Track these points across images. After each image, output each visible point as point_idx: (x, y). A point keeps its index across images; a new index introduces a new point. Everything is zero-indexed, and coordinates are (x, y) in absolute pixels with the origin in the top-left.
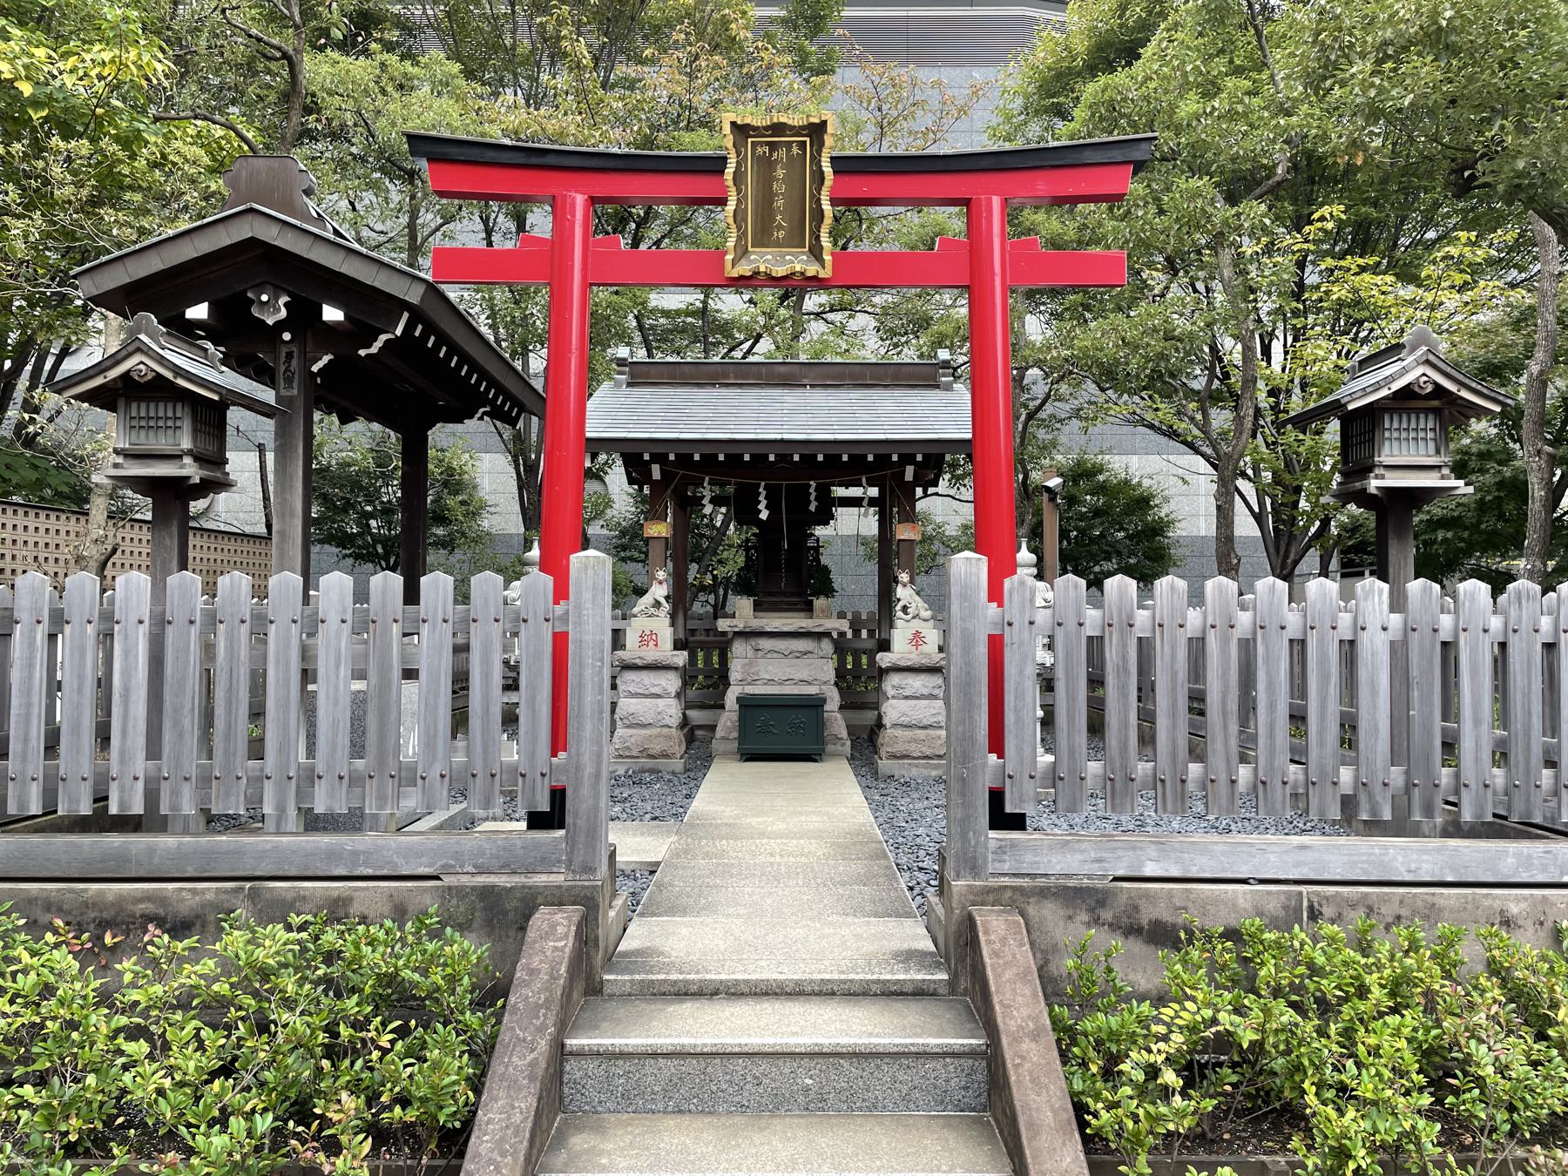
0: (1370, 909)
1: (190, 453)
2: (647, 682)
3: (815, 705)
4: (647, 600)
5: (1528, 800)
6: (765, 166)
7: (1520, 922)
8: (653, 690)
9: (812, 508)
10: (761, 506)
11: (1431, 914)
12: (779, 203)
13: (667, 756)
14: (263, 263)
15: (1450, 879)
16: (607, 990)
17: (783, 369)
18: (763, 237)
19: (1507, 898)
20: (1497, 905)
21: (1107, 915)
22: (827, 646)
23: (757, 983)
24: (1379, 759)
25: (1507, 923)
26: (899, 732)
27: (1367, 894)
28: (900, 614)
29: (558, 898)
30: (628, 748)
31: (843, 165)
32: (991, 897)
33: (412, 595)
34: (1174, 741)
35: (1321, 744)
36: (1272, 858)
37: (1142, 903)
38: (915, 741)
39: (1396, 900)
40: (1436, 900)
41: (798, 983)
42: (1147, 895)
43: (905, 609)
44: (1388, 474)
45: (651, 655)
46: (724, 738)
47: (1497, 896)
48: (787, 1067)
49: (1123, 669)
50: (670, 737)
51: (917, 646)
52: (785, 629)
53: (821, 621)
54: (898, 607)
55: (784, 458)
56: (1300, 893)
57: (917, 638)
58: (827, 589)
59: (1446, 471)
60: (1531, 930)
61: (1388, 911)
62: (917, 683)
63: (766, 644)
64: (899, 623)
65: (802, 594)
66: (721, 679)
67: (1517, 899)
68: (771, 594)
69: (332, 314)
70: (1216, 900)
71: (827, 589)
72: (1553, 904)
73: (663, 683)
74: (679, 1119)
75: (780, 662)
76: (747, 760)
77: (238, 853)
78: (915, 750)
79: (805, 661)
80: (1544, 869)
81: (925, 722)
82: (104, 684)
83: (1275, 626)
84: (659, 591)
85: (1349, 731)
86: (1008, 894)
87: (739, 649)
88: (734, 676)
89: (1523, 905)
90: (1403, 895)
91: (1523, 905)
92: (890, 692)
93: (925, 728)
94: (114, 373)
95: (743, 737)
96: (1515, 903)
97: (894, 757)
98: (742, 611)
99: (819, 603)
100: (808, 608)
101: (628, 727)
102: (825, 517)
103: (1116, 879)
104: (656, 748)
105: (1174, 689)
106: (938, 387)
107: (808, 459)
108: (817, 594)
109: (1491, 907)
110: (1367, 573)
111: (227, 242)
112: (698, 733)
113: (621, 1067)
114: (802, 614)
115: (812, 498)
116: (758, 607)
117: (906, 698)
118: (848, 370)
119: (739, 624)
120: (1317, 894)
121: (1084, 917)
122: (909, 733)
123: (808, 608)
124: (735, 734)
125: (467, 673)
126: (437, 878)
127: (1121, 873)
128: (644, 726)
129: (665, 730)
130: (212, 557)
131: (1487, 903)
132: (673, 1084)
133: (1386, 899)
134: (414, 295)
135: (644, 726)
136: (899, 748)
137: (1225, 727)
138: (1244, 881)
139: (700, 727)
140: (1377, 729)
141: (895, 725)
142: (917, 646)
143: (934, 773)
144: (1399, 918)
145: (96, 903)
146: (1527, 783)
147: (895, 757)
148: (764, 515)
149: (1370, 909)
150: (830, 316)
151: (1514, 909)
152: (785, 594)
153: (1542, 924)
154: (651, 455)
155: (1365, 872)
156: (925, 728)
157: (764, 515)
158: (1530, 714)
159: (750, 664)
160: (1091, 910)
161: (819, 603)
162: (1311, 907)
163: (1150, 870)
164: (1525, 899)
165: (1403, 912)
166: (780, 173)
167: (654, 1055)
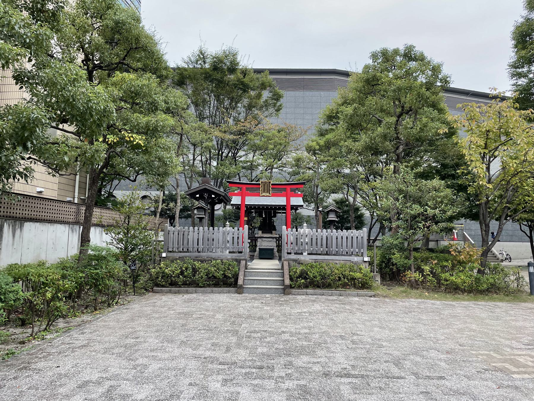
3: (273, 249)
6: (264, 185)
14: (206, 190)
22: (275, 240)
29: (243, 260)
31: (272, 184)
33: (213, 230)
55: (267, 208)
58: (275, 230)
63: (264, 239)
66: (256, 246)
69: (213, 196)
71: (275, 230)
75: (266, 242)
82: (198, 239)
85: (322, 245)
87: (259, 240)
88: (258, 245)
98: (259, 233)
99: (273, 232)
100: (271, 233)
102: (275, 216)
107: (271, 208)
119: (259, 236)
130: (49, 212)
134: (224, 195)
161: (273, 232)
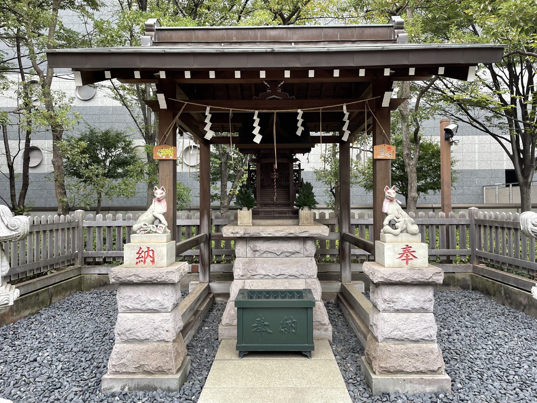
2: (143, 298)
4: (146, 217)
8: (151, 306)
9: (299, 133)
10: (256, 132)
13: (163, 372)
26: (392, 346)
28: (387, 228)
30: (124, 365)
38: (408, 355)
43: (392, 224)
45: (146, 272)
46: (228, 325)
50: (165, 353)
51: (407, 260)
52: (277, 235)
53: (307, 228)
54: (386, 222)
57: (407, 253)
62: (408, 297)
63: (262, 246)
64: (388, 237)
65: (289, 205)
68: (266, 205)
73: (159, 298)
75: (275, 262)
76: (245, 356)
78: (407, 364)
79: (294, 259)
81: (418, 336)
84: (159, 208)
92: (381, 305)
93: (417, 341)
95: (241, 337)
97: (388, 372)
99: (304, 212)
101: (127, 341)
104: (152, 364)
108: (301, 205)
110: (511, 185)
112: (218, 299)
114: (290, 222)
115: (299, 124)
116: (256, 215)
117: (397, 311)
119: (240, 231)
122: (400, 347)
123: (295, 215)
124: (235, 322)
125: (261, 188)
128: (141, 341)
129: (162, 344)
135: (141, 341)
136: (393, 363)
139: (219, 295)
141: (387, 339)
142: (407, 260)
143: (428, 389)
147: (389, 372)
148: (258, 139)
152: (277, 205)
156: (417, 341)
157: (258, 139)
159: (249, 263)
161: (304, 212)
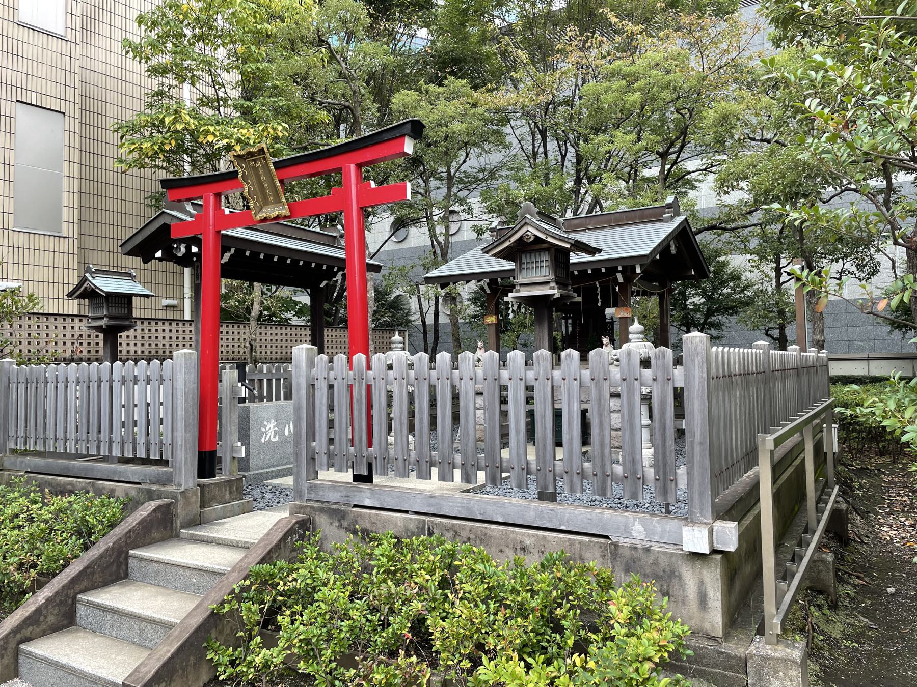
0: (456, 532)
1: (106, 316)
5: (545, 479)
7: (531, 550)
11: (485, 539)
12: (266, 185)
15: (500, 520)
16: (181, 536)
17: (576, 222)
18: (266, 203)
19: (523, 535)
20: (519, 538)
21: (345, 524)
23: (232, 541)
24: (470, 450)
25: (524, 549)
27: (454, 524)
32: (302, 511)
34: (380, 437)
35: (443, 442)
36: (418, 500)
37: (359, 519)
39: (468, 529)
40: (487, 531)
41: (237, 542)
42: (361, 515)
44: (522, 289)
47: (517, 533)
48: (188, 573)
49: (360, 401)
56: (424, 521)
59: (553, 284)
60: (537, 555)
61: (465, 534)
67: (529, 536)
70: (388, 520)
72: (548, 541)
74: (157, 588)
77: (92, 469)
80: (551, 521)
83: (422, 378)
86: (308, 509)
89: (532, 540)
90: (472, 527)
91: (532, 540)
94: (82, 288)
96: (529, 537)
103: (355, 506)
105: (380, 412)
106: (662, 220)
109: (515, 538)
111: (158, 226)
113: (143, 564)
118: (612, 217)
120: (432, 522)
121: (336, 524)
126: (139, 483)
127: (356, 503)
131: (513, 536)
132: (157, 574)
133: (463, 528)
137: (401, 431)
138: (406, 512)
140: (468, 434)
144: (469, 539)
145: (58, 485)
146: (545, 468)
149: (456, 532)
150: (714, 169)
151: (527, 542)
153: (543, 552)
154: (578, 271)
155: (460, 512)
158: (545, 428)
160: (339, 521)
162: (429, 529)
163: (367, 503)
164: (533, 536)
165: (472, 536)
166: (261, 172)
167: (156, 562)
